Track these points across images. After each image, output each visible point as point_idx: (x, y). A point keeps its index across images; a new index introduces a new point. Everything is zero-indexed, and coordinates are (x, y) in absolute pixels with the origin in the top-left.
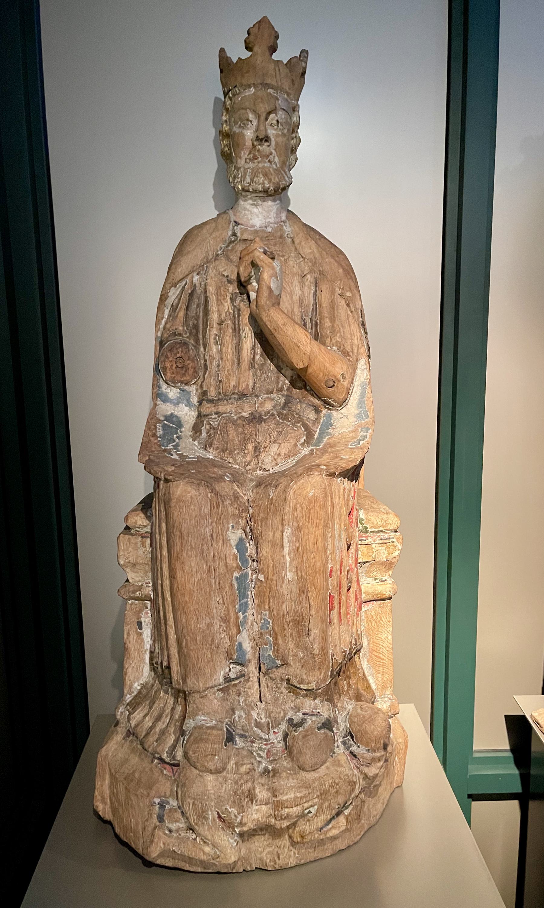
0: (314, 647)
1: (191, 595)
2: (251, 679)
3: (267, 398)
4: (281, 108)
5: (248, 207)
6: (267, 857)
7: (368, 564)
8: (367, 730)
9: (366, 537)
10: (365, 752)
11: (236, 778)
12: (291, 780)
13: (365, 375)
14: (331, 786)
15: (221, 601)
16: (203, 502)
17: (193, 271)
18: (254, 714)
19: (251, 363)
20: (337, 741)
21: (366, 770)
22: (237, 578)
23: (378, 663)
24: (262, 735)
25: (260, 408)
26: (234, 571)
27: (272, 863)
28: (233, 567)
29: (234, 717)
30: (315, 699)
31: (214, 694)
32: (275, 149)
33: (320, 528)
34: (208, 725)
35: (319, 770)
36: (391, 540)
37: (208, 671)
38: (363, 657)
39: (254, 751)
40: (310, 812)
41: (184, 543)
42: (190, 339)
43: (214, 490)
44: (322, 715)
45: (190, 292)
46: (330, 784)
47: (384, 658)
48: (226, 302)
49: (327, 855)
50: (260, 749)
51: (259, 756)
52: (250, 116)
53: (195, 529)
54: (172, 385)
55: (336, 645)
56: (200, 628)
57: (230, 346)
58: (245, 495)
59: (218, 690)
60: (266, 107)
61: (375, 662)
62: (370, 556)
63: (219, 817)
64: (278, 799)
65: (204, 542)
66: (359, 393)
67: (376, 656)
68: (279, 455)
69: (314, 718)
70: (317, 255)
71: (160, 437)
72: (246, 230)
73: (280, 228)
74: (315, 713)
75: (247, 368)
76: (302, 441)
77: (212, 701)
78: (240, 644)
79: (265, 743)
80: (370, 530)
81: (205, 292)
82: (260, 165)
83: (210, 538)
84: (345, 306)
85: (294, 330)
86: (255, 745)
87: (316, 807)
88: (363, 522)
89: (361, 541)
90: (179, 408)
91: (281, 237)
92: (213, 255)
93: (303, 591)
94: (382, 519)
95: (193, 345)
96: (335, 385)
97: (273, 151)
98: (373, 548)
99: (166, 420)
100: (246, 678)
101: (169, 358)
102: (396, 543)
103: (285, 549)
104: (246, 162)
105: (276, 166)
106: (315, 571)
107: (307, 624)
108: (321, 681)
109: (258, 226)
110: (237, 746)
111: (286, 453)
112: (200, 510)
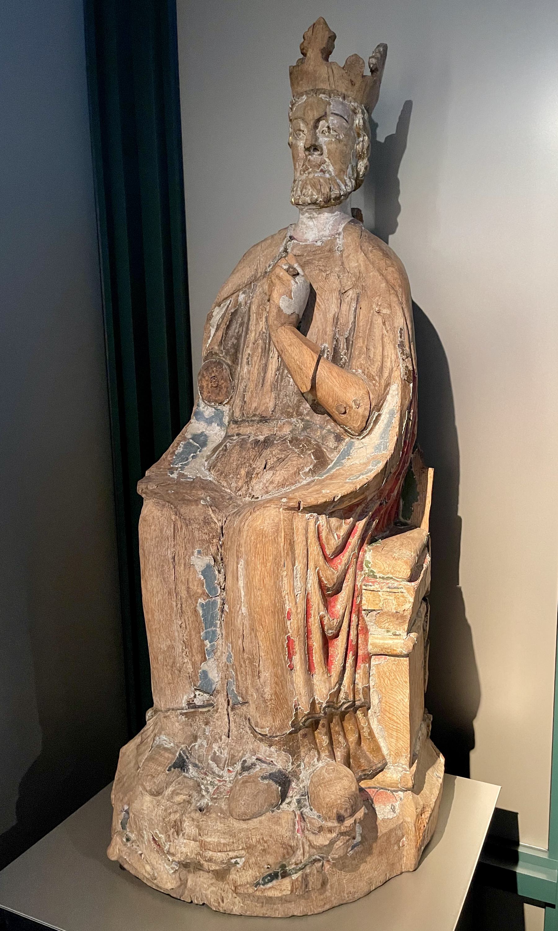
0: (266, 691)
1: (153, 615)
2: (219, 710)
3: (287, 422)
4: (332, 113)
5: (305, 220)
6: (211, 896)
7: (375, 613)
8: (320, 794)
9: (373, 582)
10: (315, 817)
11: (168, 805)
12: (218, 823)
13: (395, 401)
14: (259, 842)
15: (183, 625)
16: (165, 524)
17: (239, 290)
18: (215, 747)
19: (275, 385)
20: (292, 797)
21: (311, 837)
22: (202, 606)
23: (391, 726)
24: (216, 770)
25: (278, 432)
26: (199, 597)
27: (217, 904)
28: (196, 593)
29: (193, 744)
30: (270, 746)
31: (177, 716)
32: (328, 158)
33: (269, 564)
34: (166, 746)
35: (250, 821)
36: (399, 590)
37: (168, 692)
38: (372, 715)
39: (203, 784)
40: (236, 863)
41: (146, 562)
42: (226, 359)
43: (178, 513)
44: (275, 765)
45: (233, 311)
46: (258, 840)
47: (399, 722)
48: (262, 321)
49: (277, 915)
50: (212, 784)
51: (207, 791)
52: (302, 125)
53: (156, 550)
54: (208, 403)
55: (300, 694)
56: (161, 649)
57: (257, 367)
58: (219, 521)
59: (181, 714)
60: (315, 113)
61: (387, 723)
62: (377, 604)
63: (154, 839)
64: (202, 839)
65: (164, 564)
66: (385, 422)
67: (389, 718)
68: (272, 482)
69: (264, 766)
70: (363, 269)
71: (176, 455)
72: (298, 245)
73: (333, 241)
74: (268, 762)
75: (270, 389)
76: (307, 470)
77: (173, 724)
78: (205, 673)
79: (218, 778)
80: (378, 575)
81: (249, 311)
82: (311, 176)
83: (171, 561)
84: (382, 324)
85: (301, 351)
86: (208, 778)
87: (243, 859)
88: (370, 565)
89: (366, 586)
90: (211, 427)
91: (331, 250)
92: (261, 273)
93: (253, 630)
94: (389, 565)
95: (228, 365)
96: (347, 411)
97: (327, 160)
98: (380, 596)
99: (192, 439)
100: (215, 708)
101: (205, 377)
102: (406, 594)
103: (240, 583)
104: (300, 174)
105: (330, 175)
106: (262, 611)
107: (257, 665)
108: (276, 728)
109: (311, 240)
110: (187, 775)
111: (280, 481)
112: (161, 531)
